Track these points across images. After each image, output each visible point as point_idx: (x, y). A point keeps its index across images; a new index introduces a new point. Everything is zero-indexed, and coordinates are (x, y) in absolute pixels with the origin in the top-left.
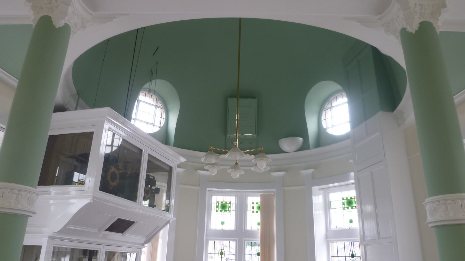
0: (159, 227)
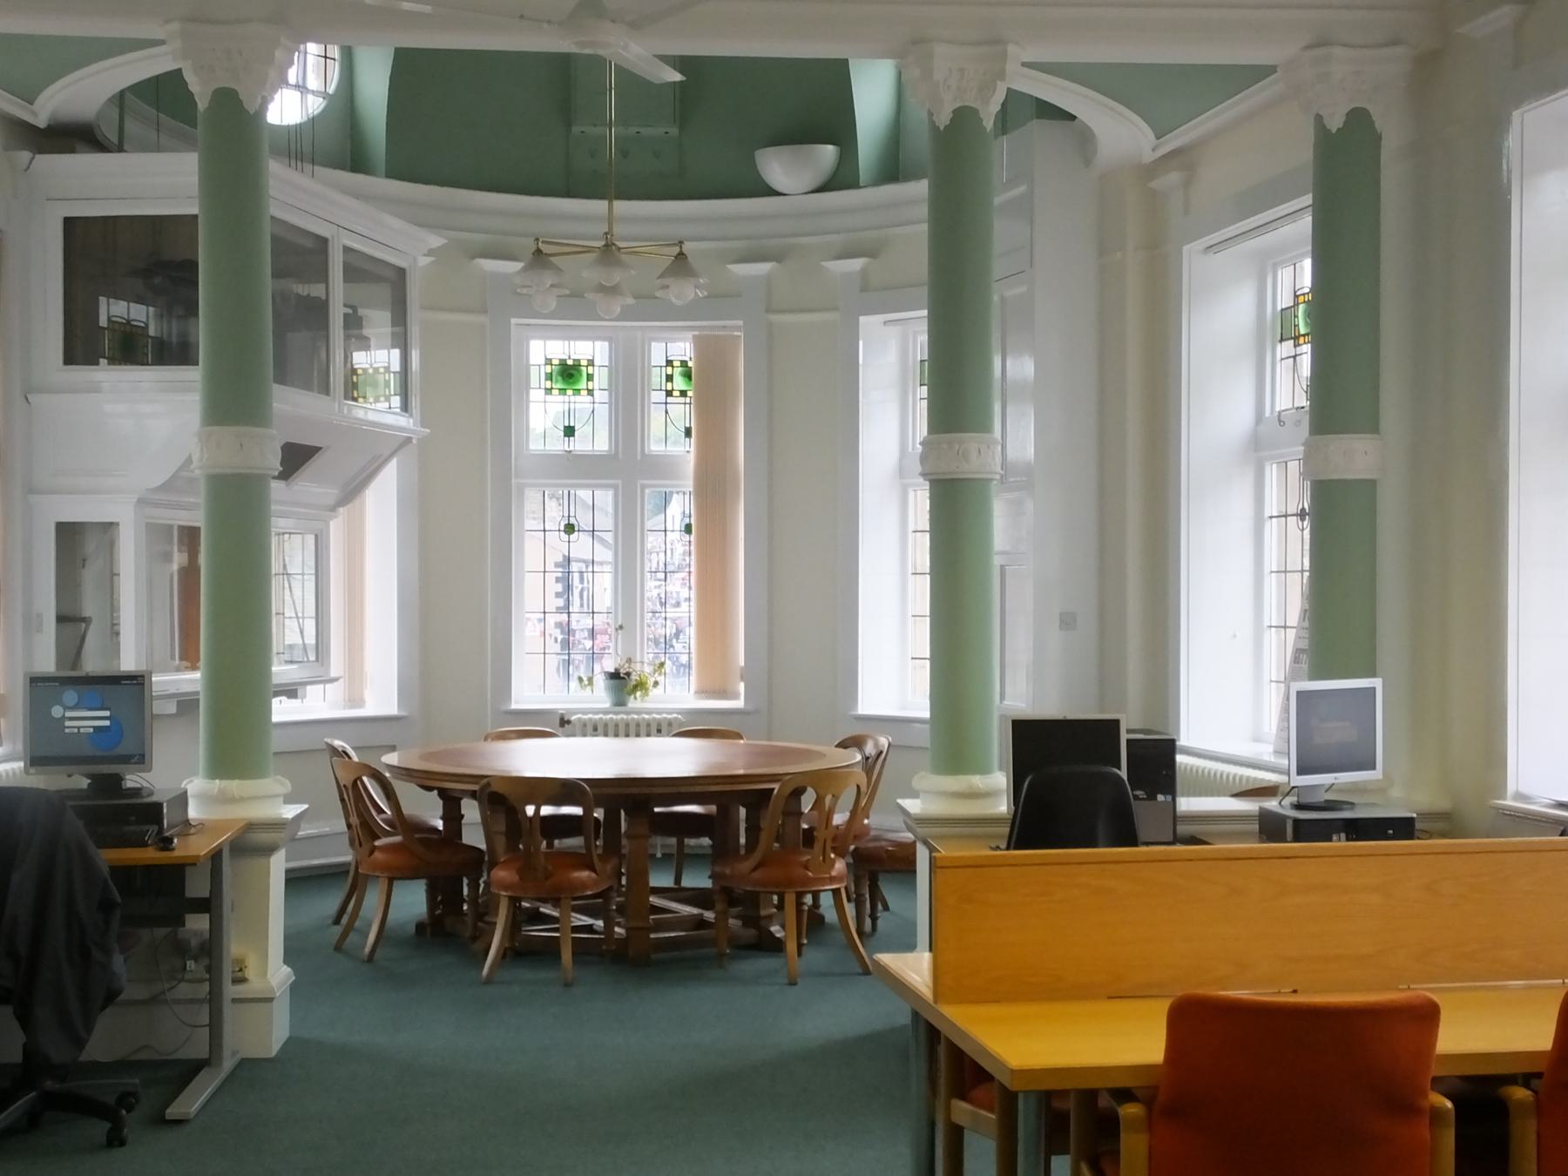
0: (381, 455)
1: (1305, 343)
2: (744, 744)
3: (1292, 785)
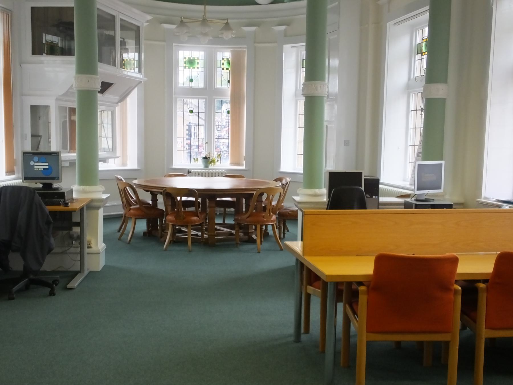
1: (425, 55)
2: (245, 180)
3: (415, 193)
